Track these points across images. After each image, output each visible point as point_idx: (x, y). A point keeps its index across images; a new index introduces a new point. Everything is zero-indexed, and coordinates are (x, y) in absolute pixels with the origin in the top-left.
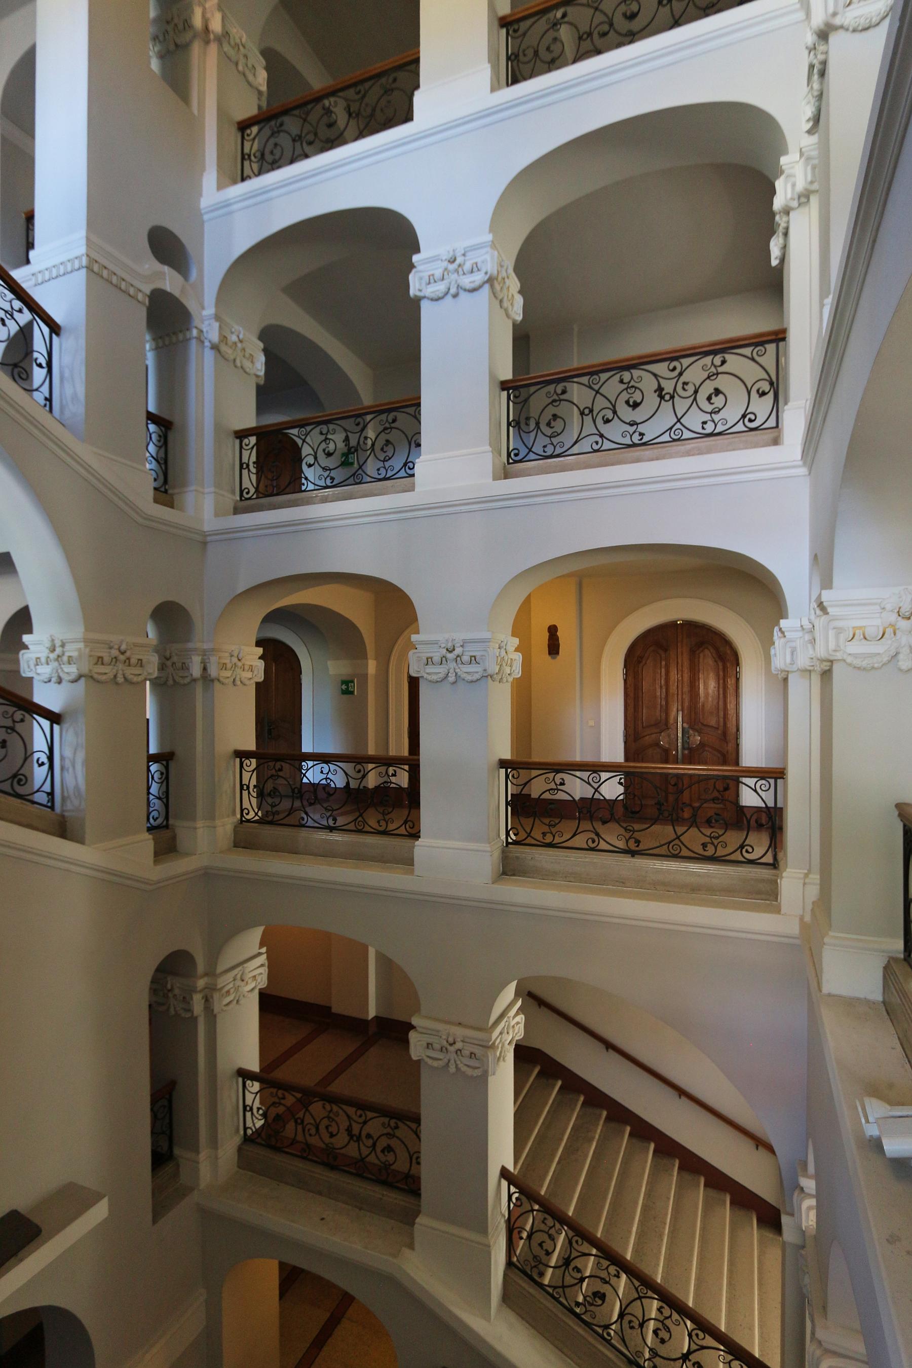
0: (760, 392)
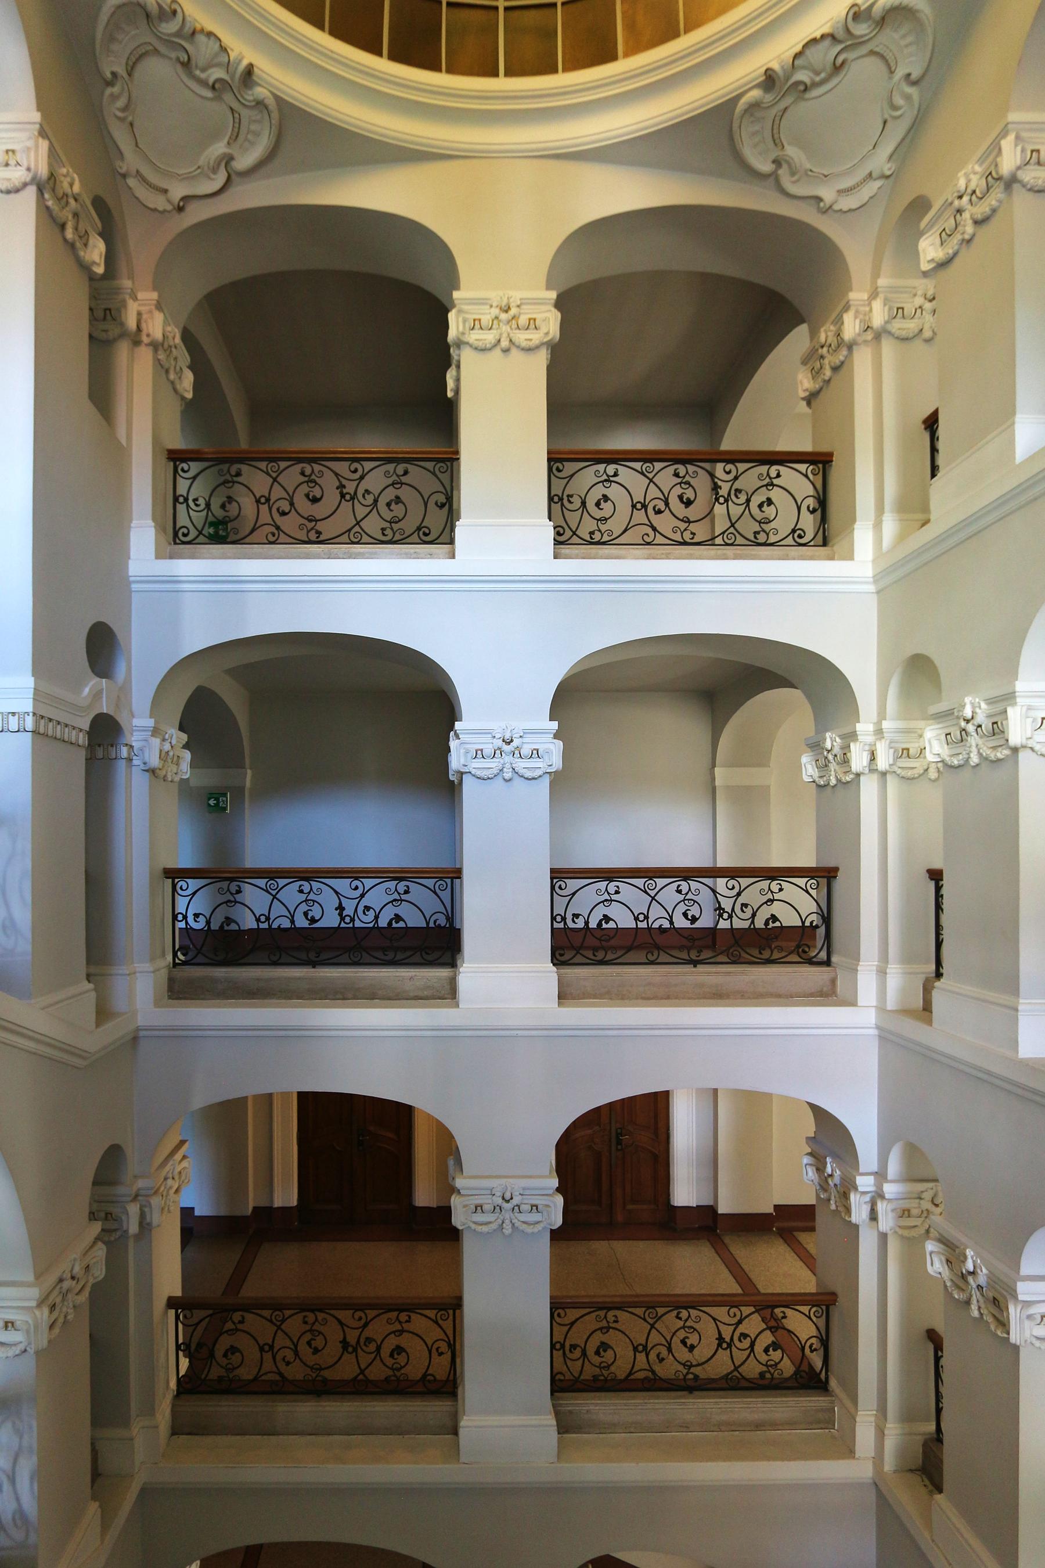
0: (811, 509)
